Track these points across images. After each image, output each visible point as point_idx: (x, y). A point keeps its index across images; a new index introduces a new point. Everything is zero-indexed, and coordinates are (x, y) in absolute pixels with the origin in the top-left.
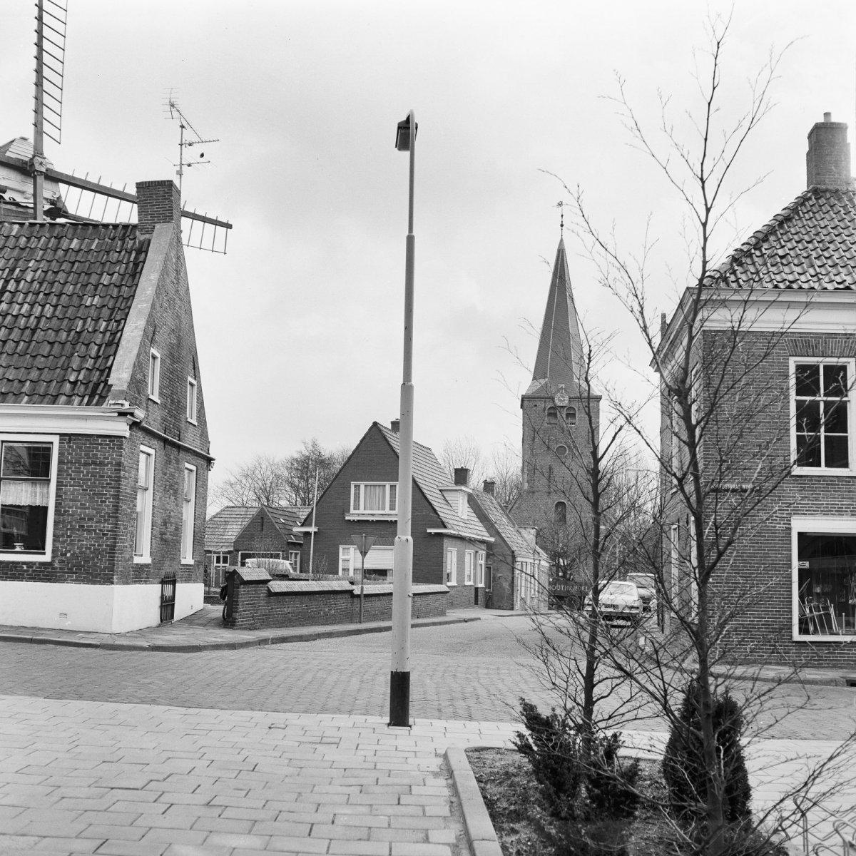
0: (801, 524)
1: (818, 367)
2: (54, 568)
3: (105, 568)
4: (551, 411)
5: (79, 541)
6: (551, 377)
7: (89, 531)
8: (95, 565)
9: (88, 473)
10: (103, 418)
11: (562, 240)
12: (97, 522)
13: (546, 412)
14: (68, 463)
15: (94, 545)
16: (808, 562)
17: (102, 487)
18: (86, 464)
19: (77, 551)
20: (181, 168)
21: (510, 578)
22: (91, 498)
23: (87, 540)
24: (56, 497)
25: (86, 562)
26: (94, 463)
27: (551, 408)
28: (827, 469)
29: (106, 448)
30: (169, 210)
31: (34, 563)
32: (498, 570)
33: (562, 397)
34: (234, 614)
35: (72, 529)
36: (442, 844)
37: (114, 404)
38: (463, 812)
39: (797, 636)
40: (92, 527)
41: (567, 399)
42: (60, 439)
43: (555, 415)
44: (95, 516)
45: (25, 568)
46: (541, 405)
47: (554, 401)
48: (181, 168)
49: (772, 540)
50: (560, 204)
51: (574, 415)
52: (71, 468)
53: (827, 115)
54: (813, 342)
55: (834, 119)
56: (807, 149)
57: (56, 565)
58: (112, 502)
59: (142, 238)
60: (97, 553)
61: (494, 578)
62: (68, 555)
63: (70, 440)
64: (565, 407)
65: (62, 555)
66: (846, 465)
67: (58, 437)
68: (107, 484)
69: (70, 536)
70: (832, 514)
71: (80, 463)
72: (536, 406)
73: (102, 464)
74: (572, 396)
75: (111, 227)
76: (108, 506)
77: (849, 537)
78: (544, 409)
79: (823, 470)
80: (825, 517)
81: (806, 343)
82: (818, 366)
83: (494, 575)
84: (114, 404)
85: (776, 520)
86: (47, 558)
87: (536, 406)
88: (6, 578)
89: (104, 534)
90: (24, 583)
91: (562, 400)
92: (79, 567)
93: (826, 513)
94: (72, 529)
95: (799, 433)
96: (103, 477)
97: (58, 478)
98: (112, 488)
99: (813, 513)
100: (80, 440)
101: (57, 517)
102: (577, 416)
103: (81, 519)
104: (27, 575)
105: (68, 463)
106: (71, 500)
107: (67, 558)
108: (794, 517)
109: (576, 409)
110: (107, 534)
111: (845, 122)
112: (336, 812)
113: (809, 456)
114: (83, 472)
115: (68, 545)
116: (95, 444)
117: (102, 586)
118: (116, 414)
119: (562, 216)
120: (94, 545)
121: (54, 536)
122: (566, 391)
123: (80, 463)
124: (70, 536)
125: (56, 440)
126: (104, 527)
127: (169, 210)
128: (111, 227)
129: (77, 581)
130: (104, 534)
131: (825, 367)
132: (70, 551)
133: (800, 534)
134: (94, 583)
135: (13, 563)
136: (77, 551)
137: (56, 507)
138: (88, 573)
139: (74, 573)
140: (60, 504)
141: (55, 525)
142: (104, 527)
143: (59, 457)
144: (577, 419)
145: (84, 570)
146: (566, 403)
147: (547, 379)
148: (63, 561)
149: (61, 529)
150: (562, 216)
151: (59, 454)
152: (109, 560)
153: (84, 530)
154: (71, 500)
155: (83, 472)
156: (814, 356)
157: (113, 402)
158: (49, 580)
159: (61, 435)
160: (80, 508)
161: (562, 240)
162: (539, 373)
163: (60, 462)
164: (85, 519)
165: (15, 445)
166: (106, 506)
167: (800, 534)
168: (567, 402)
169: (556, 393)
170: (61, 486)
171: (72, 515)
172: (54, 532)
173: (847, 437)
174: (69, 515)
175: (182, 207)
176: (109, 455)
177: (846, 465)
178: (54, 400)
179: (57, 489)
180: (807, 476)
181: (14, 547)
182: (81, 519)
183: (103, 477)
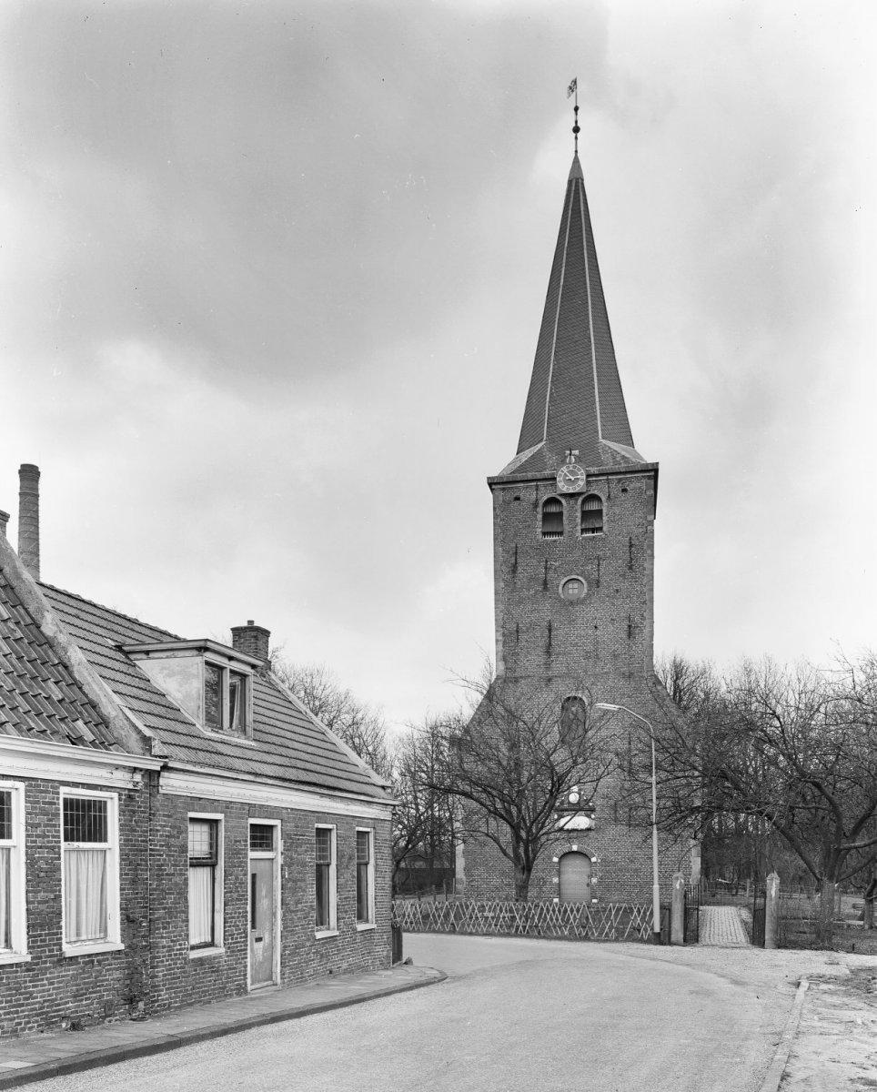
0: (316, 825)
6: (551, 440)
11: (576, 161)
33: (572, 473)
36: (222, 754)
38: (685, 919)
46: (529, 495)
64: (579, 494)
66: (106, 841)
72: (517, 499)
74: (594, 470)
78: (536, 505)
82: (271, 850)
87: (517, 499)
101: (26, 483)
112: (251, 720)
119: (576, 109)
144: (605, 518)
146: (580, 485)
161: (576, 161)
162: (528, 435)
168: (582, 483)
175: (269, 658)
177: (106, 841)
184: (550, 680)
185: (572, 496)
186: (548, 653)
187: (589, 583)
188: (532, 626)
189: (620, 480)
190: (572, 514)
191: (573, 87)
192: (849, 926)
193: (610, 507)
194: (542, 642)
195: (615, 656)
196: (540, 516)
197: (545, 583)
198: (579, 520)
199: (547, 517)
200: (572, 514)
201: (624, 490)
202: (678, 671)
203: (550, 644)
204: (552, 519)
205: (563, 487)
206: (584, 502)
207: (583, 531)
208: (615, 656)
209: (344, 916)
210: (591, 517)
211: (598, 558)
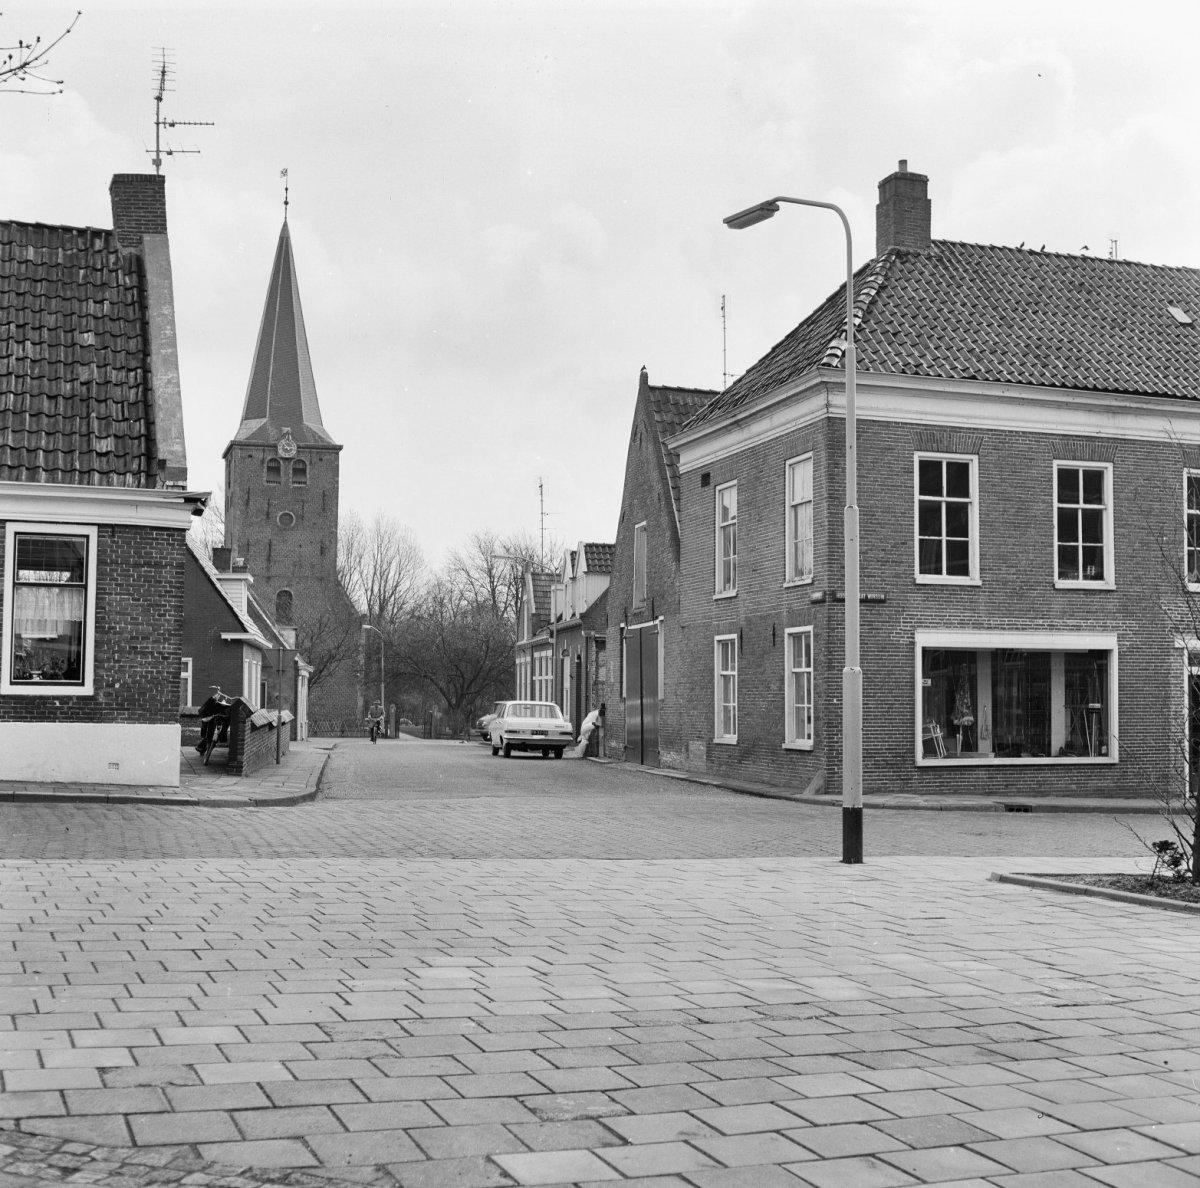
0: (926, 638)
1: (940, 463)
2: (97, 704)
3: (167, 702)
4: (273, 465)
5: (131, 667)
6: (272, 418)
7: (144, 654)
8: (153, 698)
9: (139, 577)
10: (171, 506)
11: (285, 225)
12: (154, 642)
13: (265, 465)
14: (111, 563)
15: (152, 672)
16: (191, 659)
17: (160, 596)
18: (137, 565)
19: (130, 681)
20: (158, 155)
21: (292, 698)
22: (146, 611)
23: (142, 667)
24: (97, 609)
25: (140, 694)
26: (148, 564)
27: (271, 460)
28: (948, 577)
29: (163, 544)
30: (160, 216)
31: (70, 698)
32: (274, 687)
33: (288, 445)
34: (239, 757)
35: (121, 651)
37: (173, 486)
39: (921, 761)
40: (148, 648)
41: (294, 448)
42: (99, 532)
43: (277, 470)
44: (151, 634)
45: (58, 704)
46: (258, 455)
47: (277, 452)
48: (158, 155)
49: (892, 656)
50: (284, 173)
51: (303, 471)
52: (117, 570)
53: (903, 163)
54: (938, 436)
55: (911, 169)
56: (878, 202)
57: (101, 699)
58: (173, 616)
59: (126, 252)
60: (156, 682)
61: (269, 698)
62: (117, 686)
63: (113, 532)
64: (291, 459)
65: (107, 686)
66: (921, 573)
67: (95, 528)
68: (166, 592)
69: (118, 661)
70: (1017, 629)
71: (128, 564)
73: (157, 565)
74: (301, 444)
75: (75, 232)
76: (168, 621)
77: (965, 652)
78: (263, 462)
79: (944, 579)
80: (947, 631)
81: (930, 436)
83: (269, 693)
84: (173, 486)
85: (900, 633)
86: (87, 690)
88: (31, 718)
89: (164, 658)
90: (58, 724)
91: (287, 449)
92: (132, 701)
93: (948, 625)
94: (121, 651)
95: (922, 537)
96: (160, 582)
97: (97, 584)
98: (173, 597)
99: (935, 625)
100: (125, 532)
102: (308, 472)
103: (132, 638)
104: (61, 713)
105: (111, 563)
106: (117, 613)
107: (117, 691)
108: (919, 630)
109: (307, 463)
110: (168, 658)
111: (925, 174)
113: (930, 564)
114: (133, 576)
115: (116, 672)
116: (149, 539)
117: (165, 725)
118: (183, 501)
119: (287, 189)
120: (152, 672)
121: (96, 660)
122: (294, 438)
123: (128, 564)
124: (118, 661)
125: (93, 532)
126: (164, 648)
127: (160, 216)
128: (75, 232)
129: (131, 720)
130: (164, 658)
131: (948, 464)
132: (119, 681)
133: (925, 650)
134: (153, 721)
135: (41, 697)
136: (130, 681)
137: (96, 623)
138: (144, 710)
139: (126, 709)
140: (103, 618)
141: (96, 647)
142: (164, 648)
143: (98, 555)
145: (140, 705)
147: (264, 420)
148: (110, 694)
149: (105, 652)
150: (287, 189)
151: (98, 551)
152: (173, 692)
153: (136, 653)
154: (117, 613)
155: (133, 576)
156: (938, 451)
157: (171, 483)
158: (91, 720)
159: (100, 526)
160: (130, 624)
161: (285, 225)
162: (253, 410)
163: (100, 562)
164: (138, 638)
165: (28, 537)
166: (165, 620)
167: (925, 650)
169: (278, 440)
170: (102, 594)
171: (120, 633)
172: (95, 656)
173: (967, 542)
174: (115, 633)
176: (168, 554)
177: (921, 573)
178: (33, 475)
179: (97, 598)
180: (930, 585)
181: (31, 677)
182: (132, 638)
183: (160, 582)
184: (269, 578)
185: (287, 459)
186: (269, 560)
187: (297, 516)
188: (258, 542)
189: (318, 453)
190: (287, 471)
191: (284, 173)
192: (601, 644)
193: (311, 469)
194: (265, 553)
195: (313, 566)
196: (265, 470)
197: (268, 514)
198: (291, 476)
199: (269, 469)
200: (287, 471)
201: (321, 460)
202: (893, 1010)
203: (270, 555)
204: (274, 469)
205: (281, 453)
206: (295, 463)
207: (294, 482)
208: (313, 566)
209: (1010, 490)
210: (300, 471)
211: (302, 501)
